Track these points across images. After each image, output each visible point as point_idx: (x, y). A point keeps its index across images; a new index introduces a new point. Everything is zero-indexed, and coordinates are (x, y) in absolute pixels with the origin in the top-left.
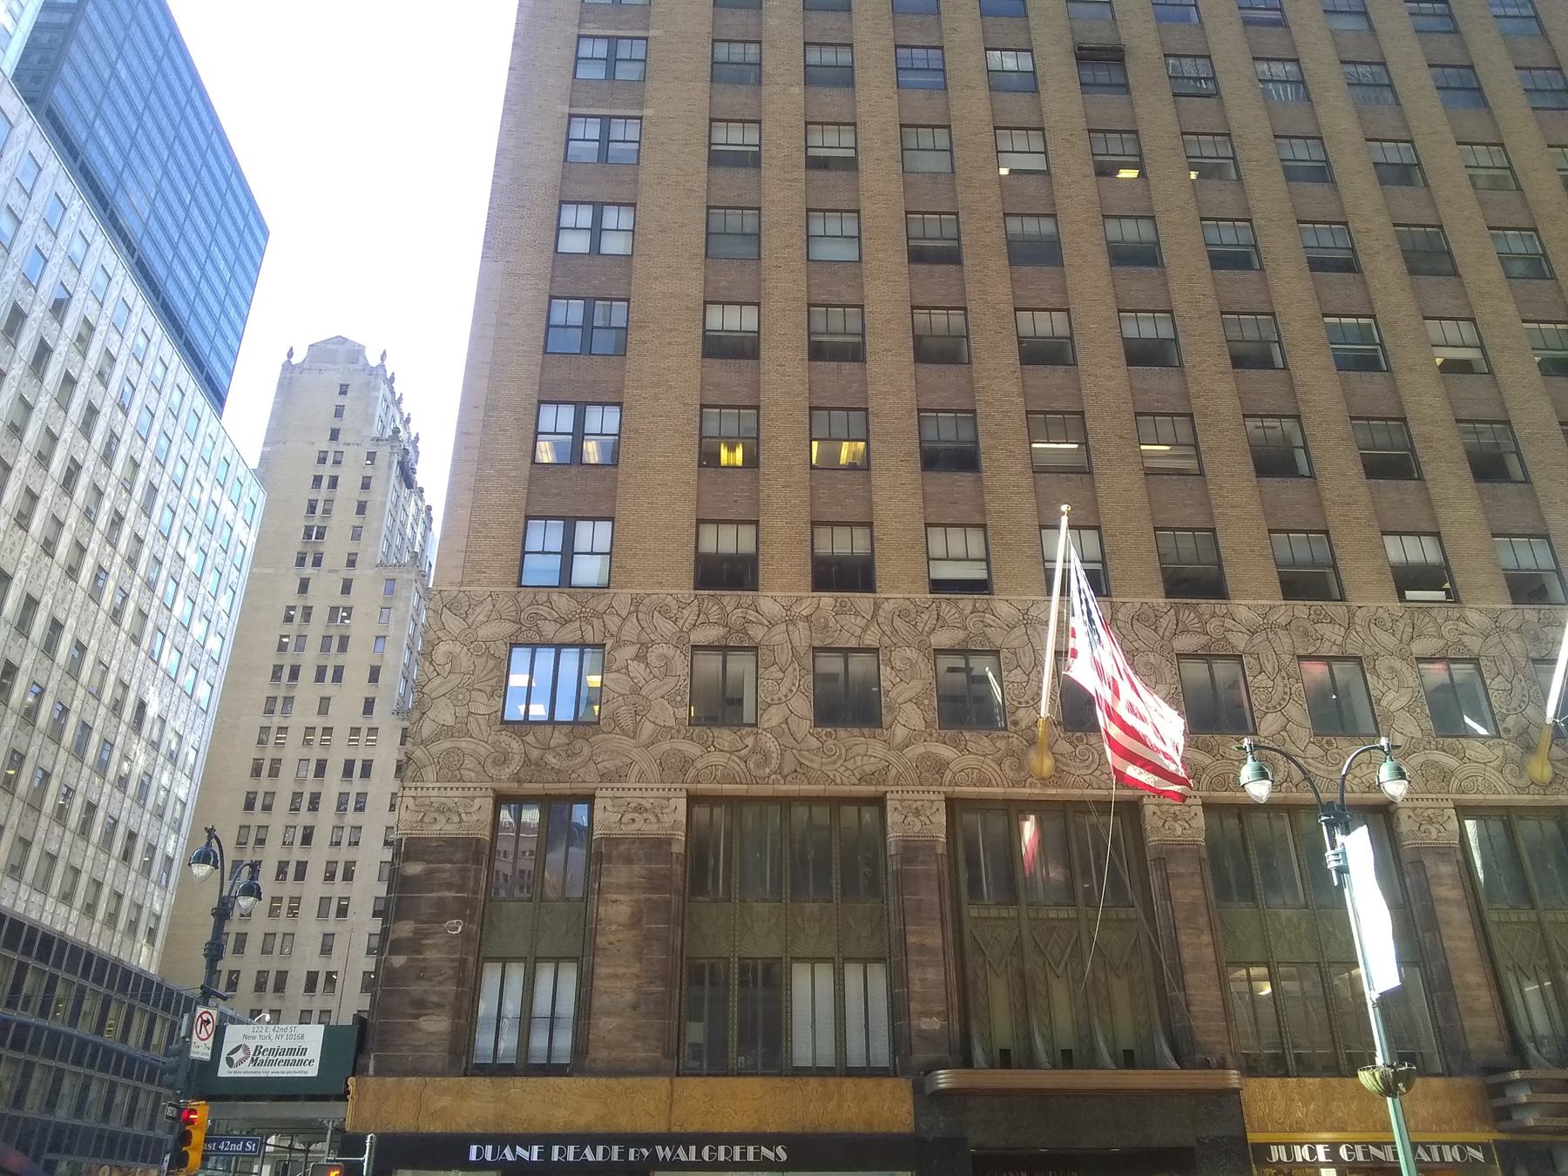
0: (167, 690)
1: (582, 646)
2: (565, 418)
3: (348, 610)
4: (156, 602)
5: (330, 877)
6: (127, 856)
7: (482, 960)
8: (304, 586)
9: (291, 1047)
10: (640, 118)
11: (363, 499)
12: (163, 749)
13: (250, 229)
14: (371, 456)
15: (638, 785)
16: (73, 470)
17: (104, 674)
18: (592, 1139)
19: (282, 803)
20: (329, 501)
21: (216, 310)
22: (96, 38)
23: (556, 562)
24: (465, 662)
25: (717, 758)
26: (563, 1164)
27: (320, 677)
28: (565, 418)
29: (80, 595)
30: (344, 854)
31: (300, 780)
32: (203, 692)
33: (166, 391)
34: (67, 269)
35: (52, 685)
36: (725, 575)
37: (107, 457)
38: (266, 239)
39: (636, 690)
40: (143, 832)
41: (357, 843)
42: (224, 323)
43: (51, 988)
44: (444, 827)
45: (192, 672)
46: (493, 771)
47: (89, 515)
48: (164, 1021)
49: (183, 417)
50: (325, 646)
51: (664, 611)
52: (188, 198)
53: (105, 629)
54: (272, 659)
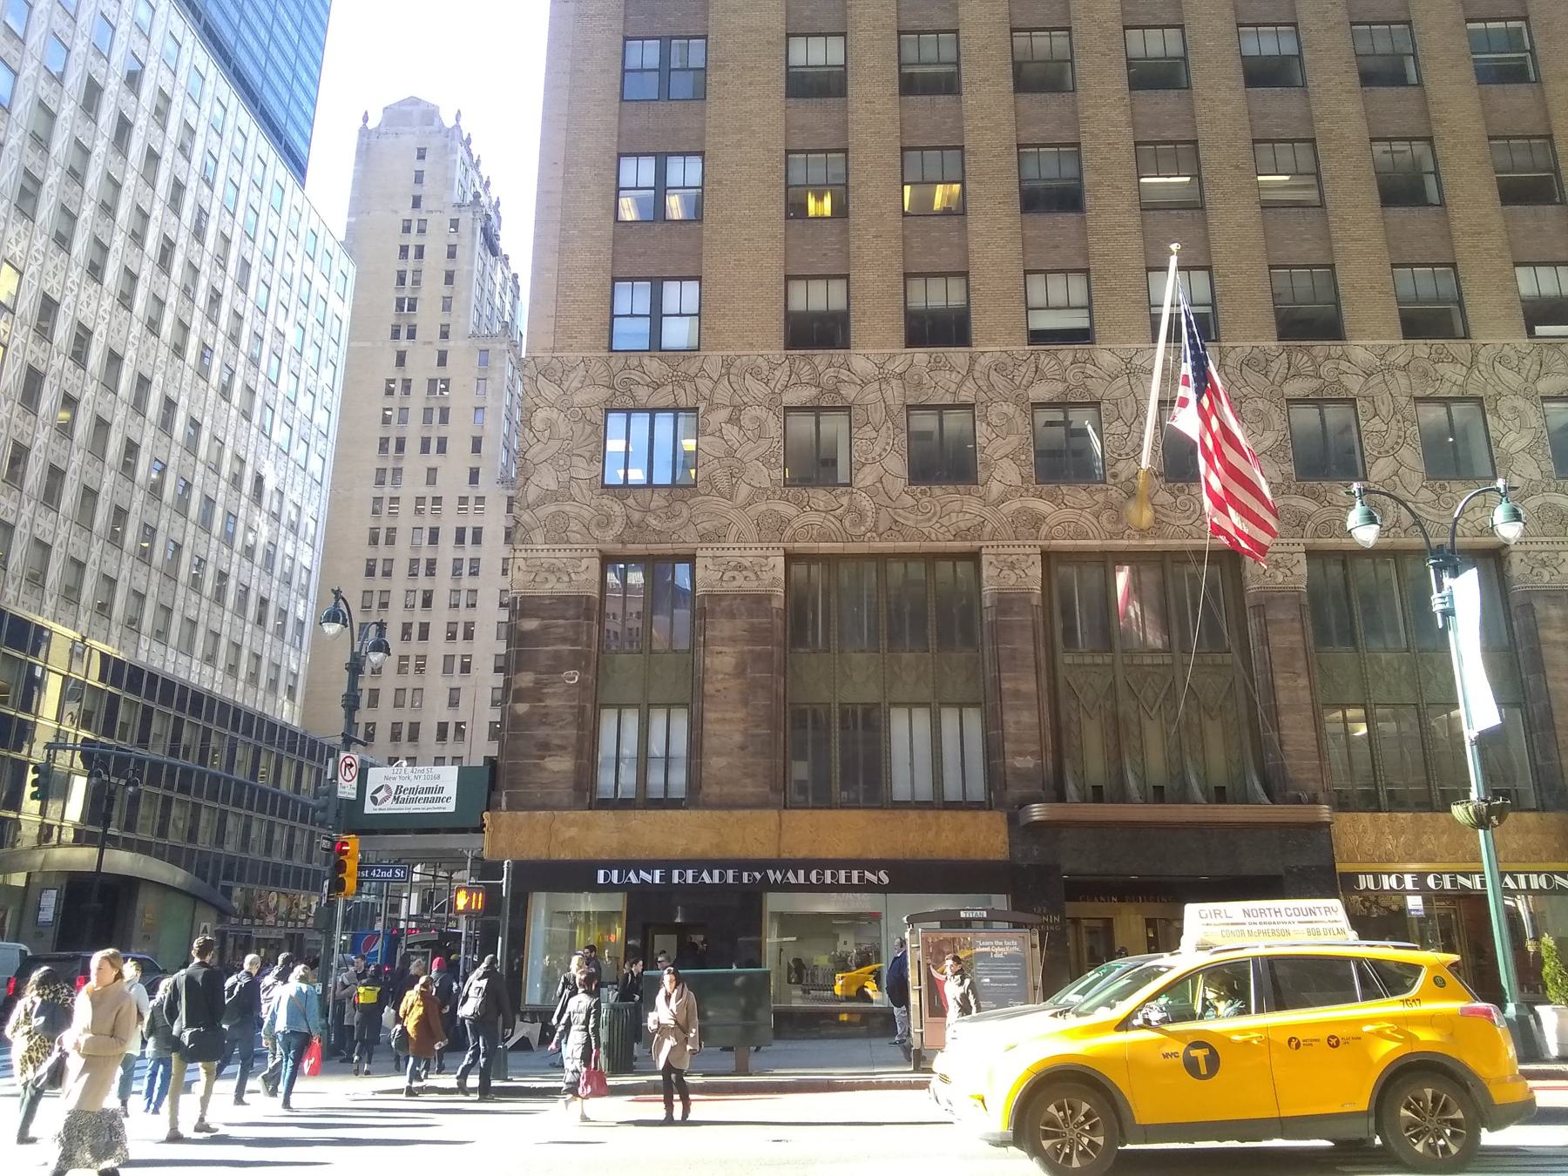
0: (281, 464)
1: (676, 410)
3: (446, 381)
4: (262, 378)
5: (452, 637)
6: (261, 620)
7: (599, 706)
8: (401, 359)
9: (433, 786)
12: (284, 519)
14: (455, 224)
16: (167, 248)
17: (220, 451)
18: (710, 865)
19: (400, 569)
20: (418, 272)
21: (288, 75)
23: (645, 325)
24: (563, 428)
26: (682, 887)
27: (425, 448)
29: (189, 373)
31: (415, 547)
32: (315, 465)
34: (135, 36)
37: (198, 234)
39: (731, 453)
41: (474, 605)
44: (552, 587)
45: (303, 445)
47: (187, 292)
48: (311, 768)
49: (267, 189)
50: (427, 420)
51: (755, 372)
53: (216, 406)
54: (378, 432)
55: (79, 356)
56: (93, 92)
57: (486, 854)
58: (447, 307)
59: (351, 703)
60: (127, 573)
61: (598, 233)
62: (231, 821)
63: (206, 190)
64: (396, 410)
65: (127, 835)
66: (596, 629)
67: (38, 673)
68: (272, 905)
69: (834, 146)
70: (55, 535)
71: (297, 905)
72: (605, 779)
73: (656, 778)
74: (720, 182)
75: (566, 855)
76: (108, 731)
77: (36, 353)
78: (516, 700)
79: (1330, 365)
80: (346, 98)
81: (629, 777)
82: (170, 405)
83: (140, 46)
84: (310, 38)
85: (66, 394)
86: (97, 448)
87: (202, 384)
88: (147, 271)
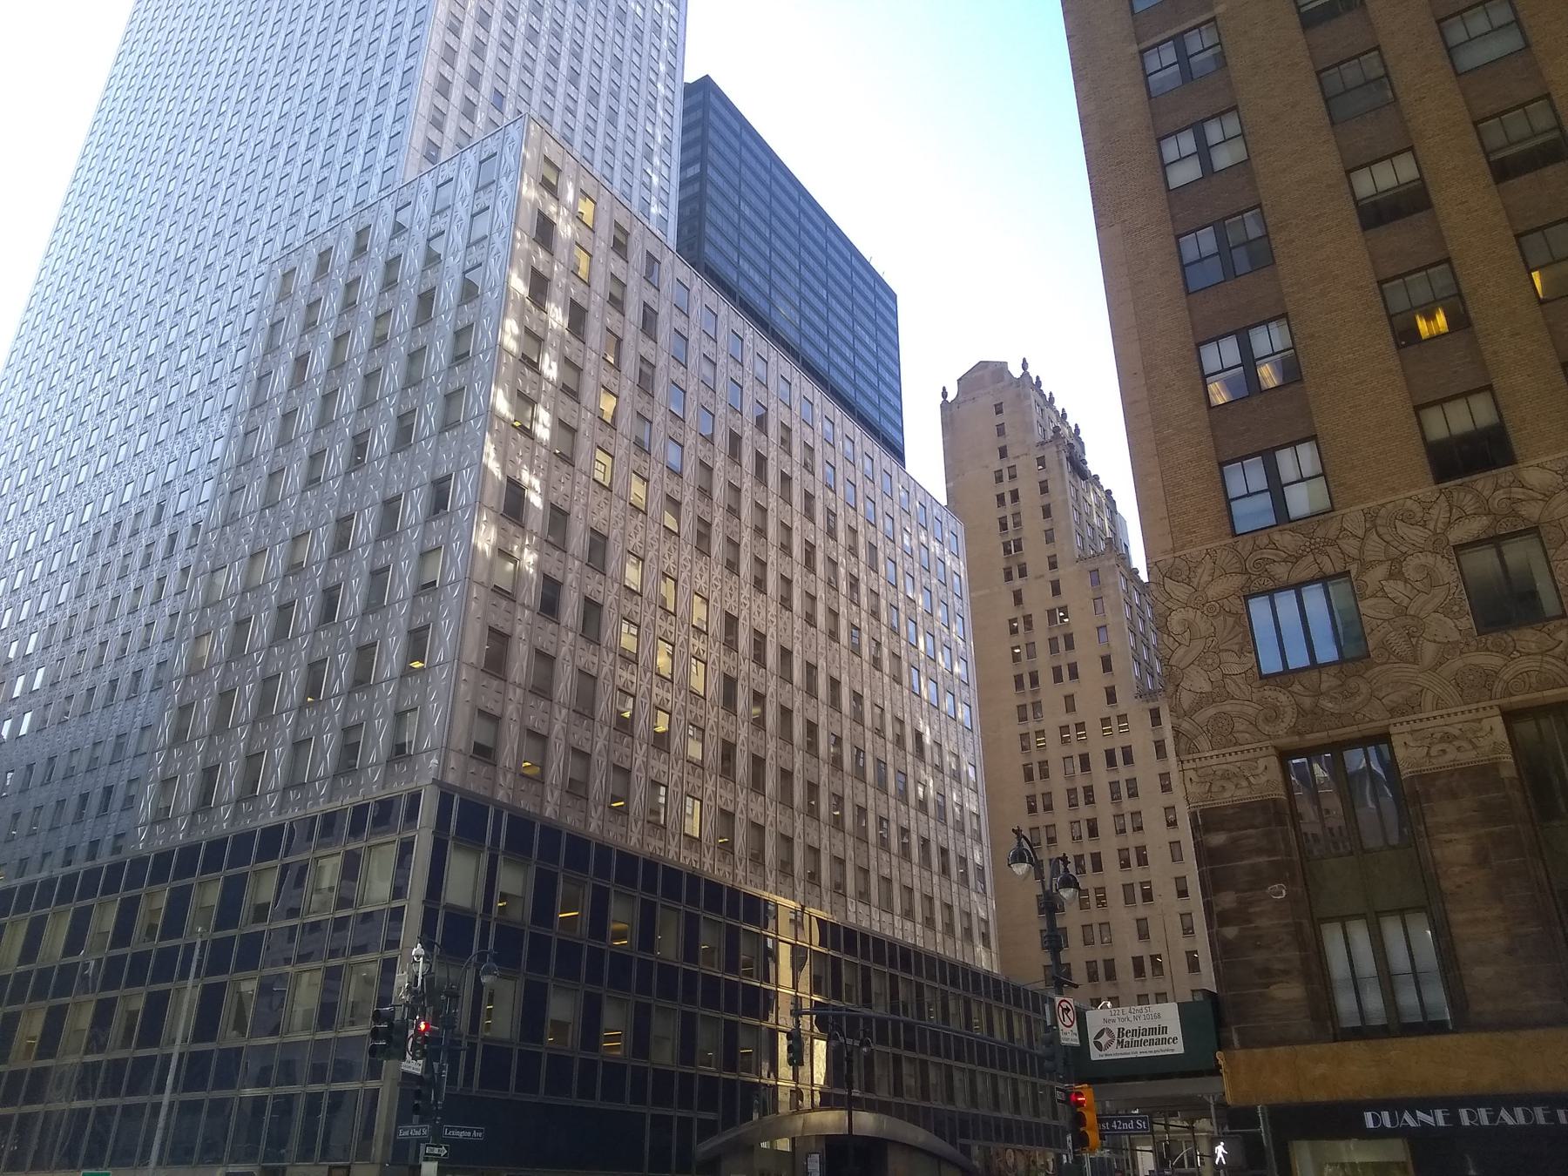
0: (934, 718)
1: (1324, 579)
2: (1230, 351)
3: (1064, 609)
5: (1125, 864)
7: (1317, 922)
8: (1018, 598)
9: (1149, 1026)
10: (1214, 19)
11: (1046, 502)
12: (946, 770)
13: (880, 298)
15: (1436, 713)
16: (810, 550)
18: (1510, 1102)
19: (1060, 800)
20: (1016, 515)
23: (1265, 501)
24: (1203, 626)
25: (1524, 664)
26: (1476, 1131)
27: (1058, 678)
28: (1230, 351)
29: (845, 652)
31: (1070, 777)
32: (963, 713)
34: (757, 388)
36: (1460, 459)
37: (831, 533)
38: (895, 302)
39: (1402, 611)
40: (952, 847)
41: (1140, 828)
43: (920, 994)
44: (1232, 794)
45: (949, 697)
46: (1267, 729)
49: (878, 479)
51: (1408, 518)
52: (824, 293)
54: (1009, 671)
55: (759, 658)
56: (735, 440)
57: (1229, 1100)
59: (1054, 941)
60: (826, 840)
63: (831, 494)
64: (1023, 646)
67: (770, 945)
68: (1011, 1162)
69: (1436, 258)
71: (1034, 1163)
72: (1345, 1003)
73: (1407, 998)
74: (1312, 336)
75: (1321, 1096)
76: (837, 995)
79: (1500, 494)
80: (925, 381)
81: (1374, 1002)
83: (761, 394)
85: (755, 692)
86: (786, 735)
87: (857, 659)
88: (797, 575)
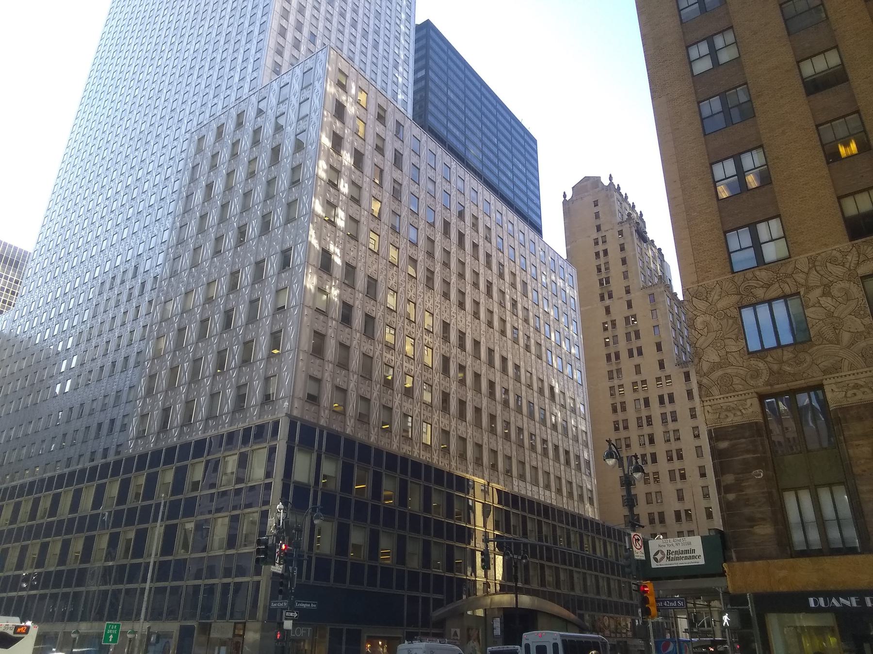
0: (560, 378)
1: (785, 297)
3: (634, 316)
4: (543, 337)
5: (670, 459)
6: (568, 462)
7: (781, 491)
8: (608, 310)
9: (690, 550)
12: (568, 407)
14: (621, 233)
16: (489, 285)
17: (531, 378)
19: (633, 424)
20: (607, 263)
21: (524, 189)
22: (437, 86)
23: (751, 253)
24: (715, 325)
27: (631, 354)
29: (510, 342)
30: (674, 446)
31: (638, 410)
32: (577, 375)
33: (516, 235)
34: (459, 195)
35: (511, 387)
37: (501, 276)
39: (830, 315)
41: (679, 439)
42: (529, 193)
44: (732, 420)
47: (502, 305)
48: (611, 543)
49: (527, 245)
50: (628, 339)
51: (833, 261)
52: (495, 140)
53: (525, 355)
54: (604, 352)
56: (447, 225)
57: (730, 590)
58: (626, 277)
59: (630, 502)
60: (500, 446)
61: (709, 210)
62: (576, 576)
63: (501, 254)
64: (611, 338)
65: (526, 586)
66: (766, 442)
68: (607, 623)
70: (467, 433)
72: (797, 537)
73: (834, 534)
75: (783, 588)
76: (508, 531)
77: (445, 348)
78: (725, 493)
80: (554, 189)
81: (814, 535)
82: (504, 360)
83: (461, 199)
84: (530, 168)
87: (517, 346)
